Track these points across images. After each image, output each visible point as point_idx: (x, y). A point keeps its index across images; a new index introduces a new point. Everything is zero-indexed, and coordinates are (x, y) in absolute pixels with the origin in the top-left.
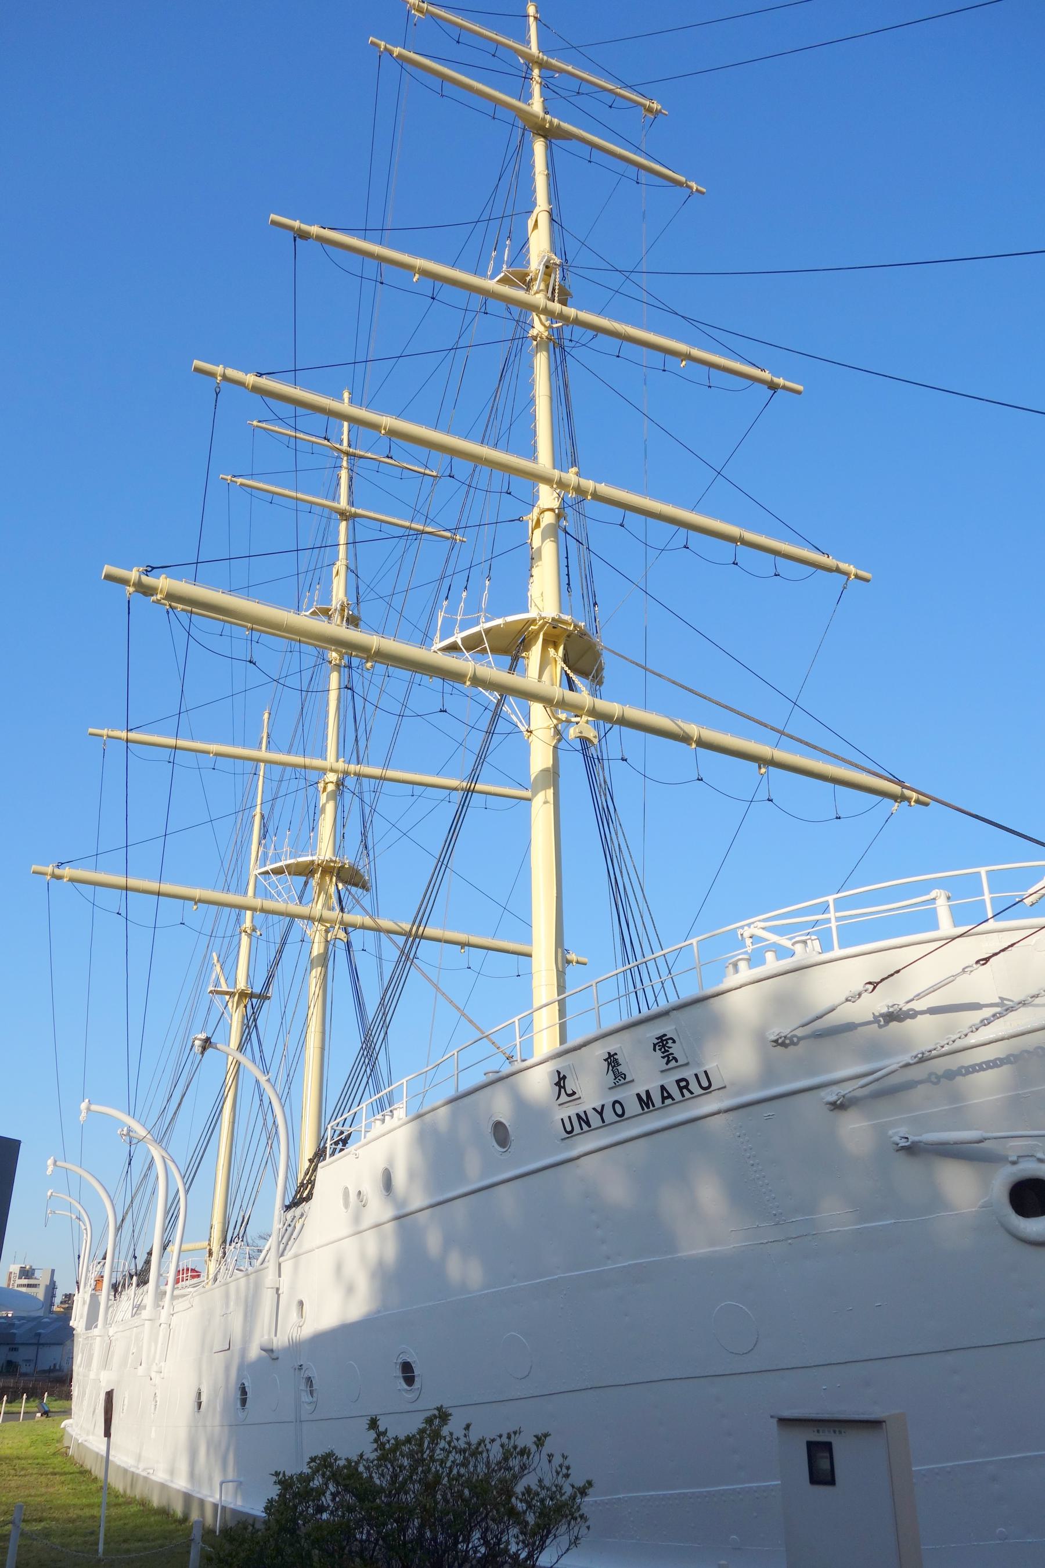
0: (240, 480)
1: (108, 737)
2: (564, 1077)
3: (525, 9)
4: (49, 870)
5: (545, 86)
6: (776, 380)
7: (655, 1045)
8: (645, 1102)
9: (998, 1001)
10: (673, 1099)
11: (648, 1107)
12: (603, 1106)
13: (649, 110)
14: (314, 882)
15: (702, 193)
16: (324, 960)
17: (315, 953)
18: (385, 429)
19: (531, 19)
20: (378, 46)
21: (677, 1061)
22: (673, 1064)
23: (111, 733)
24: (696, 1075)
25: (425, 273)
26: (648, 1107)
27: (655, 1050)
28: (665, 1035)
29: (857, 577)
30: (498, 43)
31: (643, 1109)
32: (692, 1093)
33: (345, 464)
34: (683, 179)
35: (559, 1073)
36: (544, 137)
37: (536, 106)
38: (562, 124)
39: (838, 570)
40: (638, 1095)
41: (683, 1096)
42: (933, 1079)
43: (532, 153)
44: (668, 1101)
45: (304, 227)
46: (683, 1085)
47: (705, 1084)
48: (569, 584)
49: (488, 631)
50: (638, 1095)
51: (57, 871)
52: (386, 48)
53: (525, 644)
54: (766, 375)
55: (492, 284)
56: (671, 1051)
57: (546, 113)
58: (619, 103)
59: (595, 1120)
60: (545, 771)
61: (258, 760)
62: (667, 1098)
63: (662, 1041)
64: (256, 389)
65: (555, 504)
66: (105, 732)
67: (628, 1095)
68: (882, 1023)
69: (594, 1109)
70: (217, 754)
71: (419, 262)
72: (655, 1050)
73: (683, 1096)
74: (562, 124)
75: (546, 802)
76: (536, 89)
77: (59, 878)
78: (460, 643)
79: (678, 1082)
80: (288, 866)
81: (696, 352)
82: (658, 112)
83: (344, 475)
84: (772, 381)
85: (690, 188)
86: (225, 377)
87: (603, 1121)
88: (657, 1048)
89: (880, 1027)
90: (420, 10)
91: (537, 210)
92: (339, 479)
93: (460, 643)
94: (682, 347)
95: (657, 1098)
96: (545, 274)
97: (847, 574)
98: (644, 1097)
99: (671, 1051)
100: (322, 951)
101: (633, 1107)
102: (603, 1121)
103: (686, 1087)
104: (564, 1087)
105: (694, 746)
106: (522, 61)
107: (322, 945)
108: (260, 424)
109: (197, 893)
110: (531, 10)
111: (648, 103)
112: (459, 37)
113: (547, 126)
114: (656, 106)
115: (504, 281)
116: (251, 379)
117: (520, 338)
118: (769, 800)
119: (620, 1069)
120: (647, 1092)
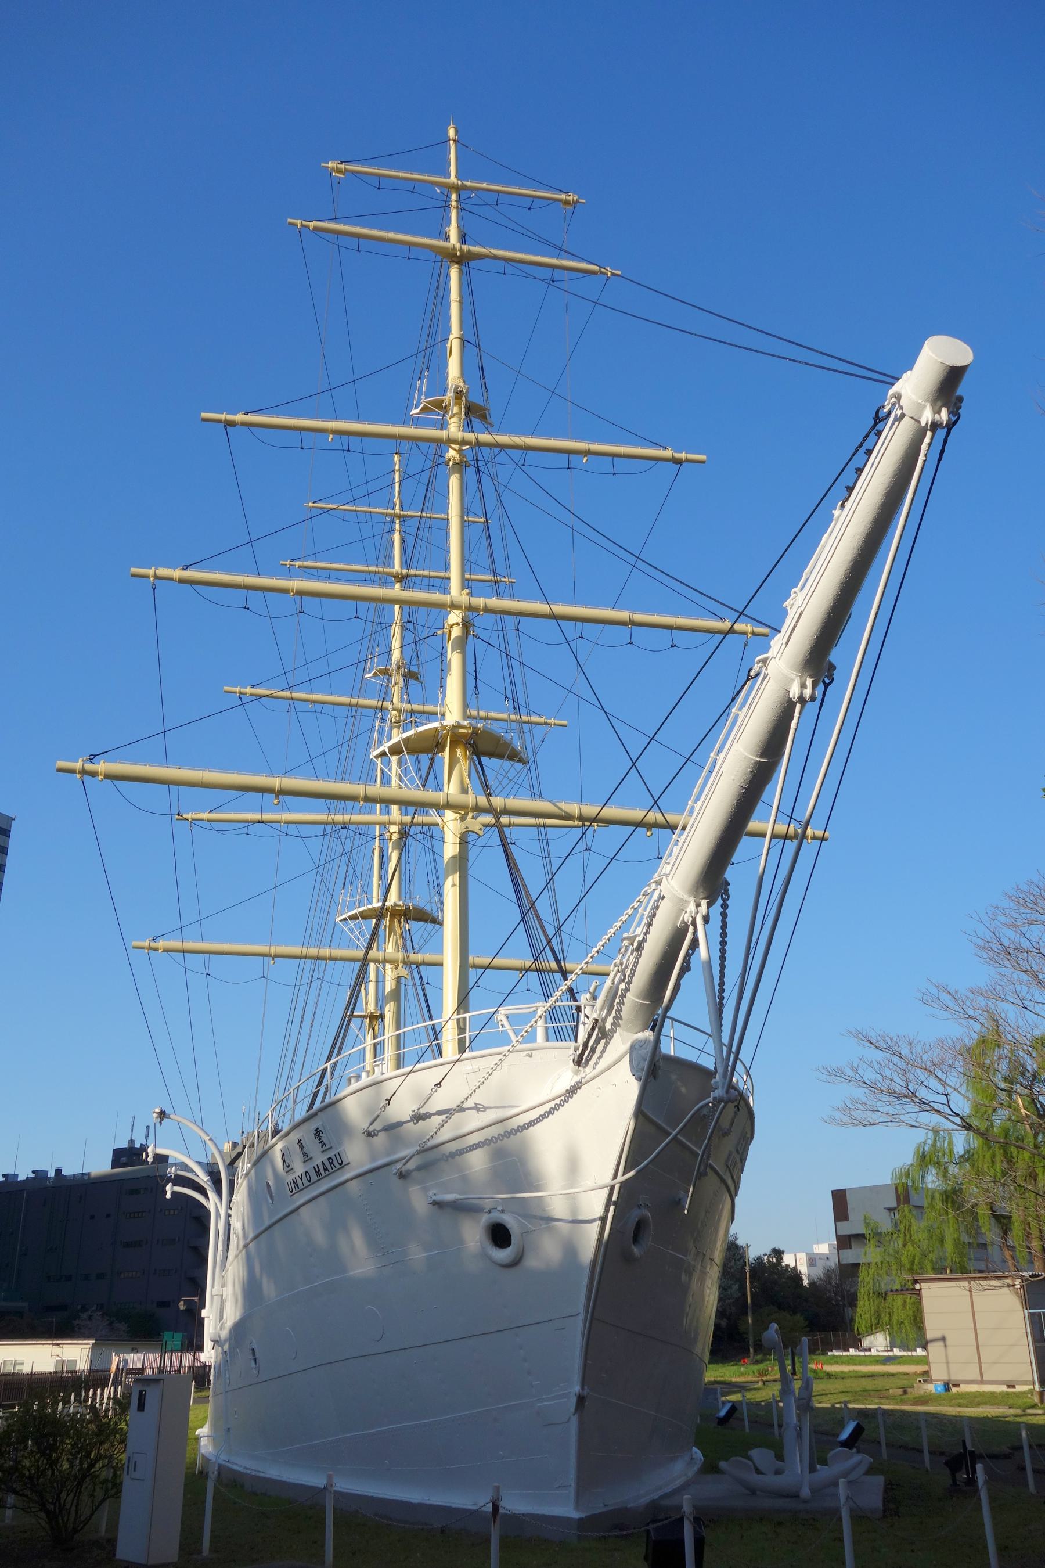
0: (298, 563)
3: (447, 132)
4: (146, 944)
5: (461, 209)
6: (678, 455)
13: (567, 203)
14: (387, 921)
16: (396, 995)
17: (388, 989)
20: (295, 225)
23: (195, 816)
25: (337, 432)
29: (754, 634)
30: (415, 180)
33: (397, 527)
36: (457, 263)
39: (546, 723)
45: (230, 417)
51: (153, 945)
52: (302, 225)
53: (439, 746)
54: (668, 453)
58: (537, 203)
60: (454, 857)
61: (375, 824)
64: (182, 581)
65: (459, 620)
71: (331, 425)
75: (453, 885)
76: (454, 214)
80: (361, 913)
83: (397, 537)
86: (156, 577)
90: (339, 171)
91: (451, 337)
92: (392, 541)
97: (745, 633)
100: (394, 987)
107: (394, 982)
108: (315, 505)
110: (452, 133)
111: (563, 197)
114: (572, 198)
116: (177, 573)
117: (438, 462)
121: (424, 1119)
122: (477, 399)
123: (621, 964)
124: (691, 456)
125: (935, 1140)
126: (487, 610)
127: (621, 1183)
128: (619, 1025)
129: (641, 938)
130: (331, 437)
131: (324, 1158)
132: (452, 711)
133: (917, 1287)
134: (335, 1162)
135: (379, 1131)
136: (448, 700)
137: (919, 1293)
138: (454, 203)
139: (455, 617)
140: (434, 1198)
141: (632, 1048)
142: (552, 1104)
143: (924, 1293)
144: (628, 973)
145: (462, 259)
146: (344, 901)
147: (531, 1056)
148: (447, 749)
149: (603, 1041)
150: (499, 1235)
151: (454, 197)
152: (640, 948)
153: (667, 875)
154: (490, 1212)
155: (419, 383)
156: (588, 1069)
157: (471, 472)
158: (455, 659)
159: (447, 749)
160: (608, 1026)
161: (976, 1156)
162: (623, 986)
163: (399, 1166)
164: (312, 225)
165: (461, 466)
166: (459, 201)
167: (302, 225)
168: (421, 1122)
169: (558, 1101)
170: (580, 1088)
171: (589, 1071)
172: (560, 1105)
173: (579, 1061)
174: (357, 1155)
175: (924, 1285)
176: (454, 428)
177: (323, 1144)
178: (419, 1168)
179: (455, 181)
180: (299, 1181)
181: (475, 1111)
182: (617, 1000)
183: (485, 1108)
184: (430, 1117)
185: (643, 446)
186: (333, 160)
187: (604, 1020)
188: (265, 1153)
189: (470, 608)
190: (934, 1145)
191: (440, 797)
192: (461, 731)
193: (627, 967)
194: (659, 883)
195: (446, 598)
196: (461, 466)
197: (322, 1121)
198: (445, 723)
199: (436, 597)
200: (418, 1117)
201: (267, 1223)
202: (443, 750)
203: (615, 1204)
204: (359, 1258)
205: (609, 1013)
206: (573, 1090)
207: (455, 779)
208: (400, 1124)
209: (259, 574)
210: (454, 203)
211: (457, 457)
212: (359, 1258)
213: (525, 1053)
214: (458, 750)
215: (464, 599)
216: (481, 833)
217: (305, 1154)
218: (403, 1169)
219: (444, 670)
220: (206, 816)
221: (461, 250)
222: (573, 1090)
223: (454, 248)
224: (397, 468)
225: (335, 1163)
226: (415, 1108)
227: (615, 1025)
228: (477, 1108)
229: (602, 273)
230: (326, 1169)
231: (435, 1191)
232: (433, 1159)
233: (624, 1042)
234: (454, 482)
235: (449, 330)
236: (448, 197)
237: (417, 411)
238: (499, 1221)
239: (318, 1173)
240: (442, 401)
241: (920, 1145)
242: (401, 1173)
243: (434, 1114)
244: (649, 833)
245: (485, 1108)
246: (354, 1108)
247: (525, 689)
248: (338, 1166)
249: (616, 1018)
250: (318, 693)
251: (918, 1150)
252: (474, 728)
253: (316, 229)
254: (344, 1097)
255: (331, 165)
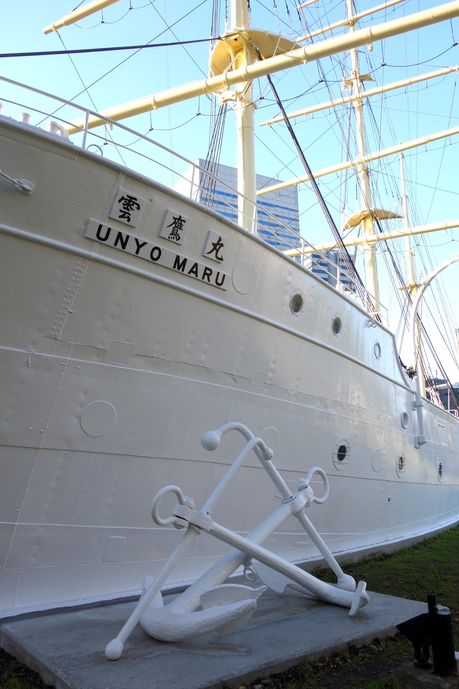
2: (222, 245)
7: (123, 198)
8: (180, 264)
10: (197, 276)
11: (179, 269)
12: (145, 244)
21: (129, 220)
22: (125, 220)
24: (218, 273)
26: (179, 269)
27: (120, 201)
28: (135, 199)
31: (174, 267)
32: (209, 280)
35: (220, 239)
40: (178, 257)
41: (203, 278)
44: (192, 275)
46: (208, 272)
47: (220, 281)
50: (178, 257)
56: (131, 212)
59: (131, 247)
62: (194, 272)
63: (130, 201)
67: (170, 252)
69: (137, 240)
72: (120, 201)
73: (203, 278)
79: (206, 269)
87: (137, 252)
88: (123, 201)
95: (188, 267)
98: (181, 262)
99: (131, 212)
101: (167, 260)
102: (137, 252)
103: (209, 275)
104: (217, 251)
119: (179, 232)
120: (185, 260)
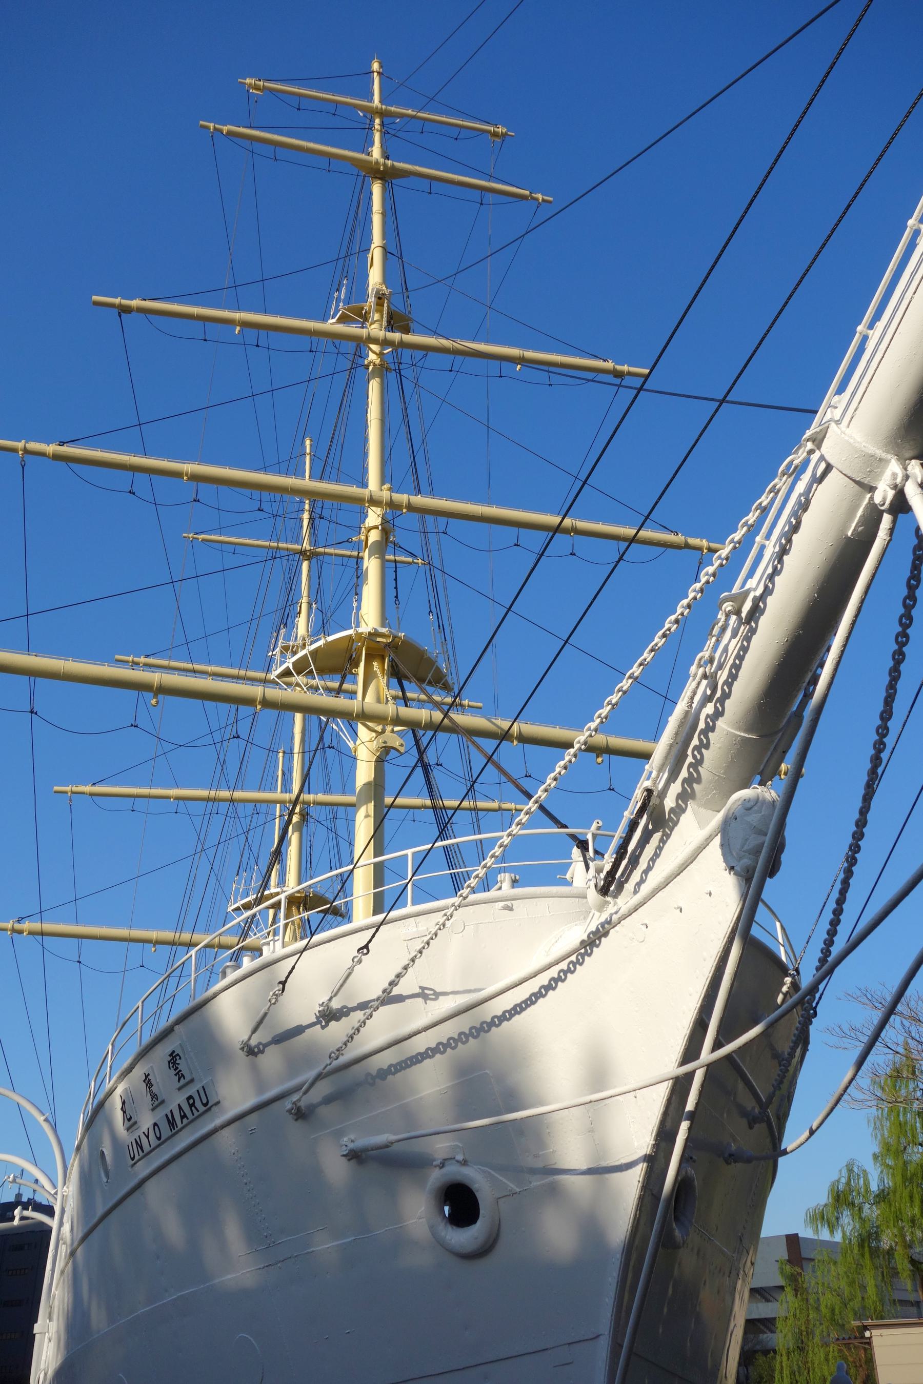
1: (73, 792)
3: (370, 66)
4: (9, 925)
5: (384, 133)
6: (619, 367)
9: (418, 991)
13: (495, 134)
15: (550, 202)
18: (187, 475)
19: (375, 74)
20: (207, 128)
23: (75, 789)
25: (245, 324)
30: (337, 103)
33: (307, 507)
34: (527, 193)
36: (380, 179)
37: (376, 153)
38: (395, 163)
39: (687, 546)
42: (370, 1080)
43: (371, 193)
48: (396, 597)
49: (314, 653)
51: (18, 926)
52: (215, 129)
54: (609, 365)
55: (331, 325)
57: (387, 158)
61: (275, 802)
64: (57, 457)
65: (378, 521)
66: (69, 789)
68: (323, 1024)
70: (178, 798)
74: (395, 163)
75: (367, 816)
76: (377, 137)
77: (20, 932)
78: (291, 668)
81: (530, 354)
82: (504, 135)
83: (306, 516)
84: (615, 370)
85: (537, 199)
86: (26, 451)
89: (323, 1028)
91: (373, 246)
93: (291, 668)
94: (515, 352)
96: (377, 304)
97: (699, 549)
105: (515, 743)
106: (361, 114)
109: (154, 935)
110: (375, 66)
112: (299, 104)
113: (382, 168)
114: (501, 130)
115: (343, 319)
116: (51, 448)
118: (610, 789)
121: (338, 1019)
122: (400, 307)
123: (711, 660)
124: (633, 369)
125: (849, 1177)
126: (411, 508)
127: (710, 1067)
128: (692, 796)
129: (758, 593)
130: (238, 328)
131: (180, 1098)
132: (369, 615)
133: (867, 1334)
134: (198, 1104)
135: (266, 1045)
136: (363, 611)
137: (869, 1342)
138: (377, 127)
139: (374, 517)
140: (351, 1146)
141: (725, 828)
142: (553, 972)
143: (875, 1342)
144: (723, 676)
145: (386, 176)
146: (237, 889)
147: (510, 909)
148: (362, 664)
149: (657, 836)
150: (460, 1203)
151: (377, 121)
152: (756, 611)
153: (838, 422)
154: (442, 1165)
155: (336, 294)
156: (621, 900)
157: (392, 376)
158: (372, 565)
159: (362, 664)
160: (669, 802)
161: (891, 1196)
162: (709, 709)
163: (295, 1097)
164: (225, 129)
165: (383, 370)
166: (382, 124)
167: (215, 129)
168: (333, 1024)
169: (564, 965)
170: (606, 934)
171: (625, 901)
172: (569, 971)
173: (609, 886)
174: (235, 1093)
175: (875, 1332)
176: (376, 329)
177: (180, 1075)
178: (328, 1100)
179: (379, 106)
180: (144, 1140)
181: (420, 1000)
182: (695, 742)
183: (437, 995)
184: (347, 1014)
185: (581, 357)
186: (251, 77)
187: (663, 793)
188: (101, 1105)
189: (392, 505)
190: (848, 1183)
191: (355, 705)
192: (378, 639)
193: (720, 667)
194: (818, 441)
195: (365, 493)
196: (383, 370)
197: (181, 1050)
198: (360, 630)
199: (353, 490)
200: (328, 1016)
201: (100, 1211)
202: (357, 666)
203: (692, 1116)
204: (236, 1263)
205: (672, 778)
206: (591, 943)
207: (372, 691)
208: (299, 1030)
209: (146, 454)
210: (377, 127)
211: (378, 361)
212: (236, 1263)
213: (502, 904)
214: (375, 664)
215: (385, 495)
216: (402, 750)
217: (154, 1096)
218: (302, 1104)
219: (359, 577)
220: (88, 789)
221: (385, 165)
222: (591, 943)
223: (377, 163)
224: (308, 451)
225: (201, 1104)
226: (325, 999)
227: (685, 796)
228: (424, 994)
229: (533, 198)
230: (184, 1116)
231: (352, 1137)
232: (351, 1082)
233: (701, 825)
234: (374, 387)
235: (370, 240)
236: (372, 121)
237: (334, 320)
238: (459, 1178)
239: (171, 1123)
240: (363, 308)
241: (834, 1183)
242: (299, 1109)
243: (354, 1009)
244: (600, 760)
245: (437, 995)
246: (232, 1012)
247: (449, 614)
248: (202, 1109)
249: (689, 781)
250: (216, 664)
251: (832, 1190)
252: (395, 637)
253: (230, 133)
254: (215, 995)
255: (248, 81)
